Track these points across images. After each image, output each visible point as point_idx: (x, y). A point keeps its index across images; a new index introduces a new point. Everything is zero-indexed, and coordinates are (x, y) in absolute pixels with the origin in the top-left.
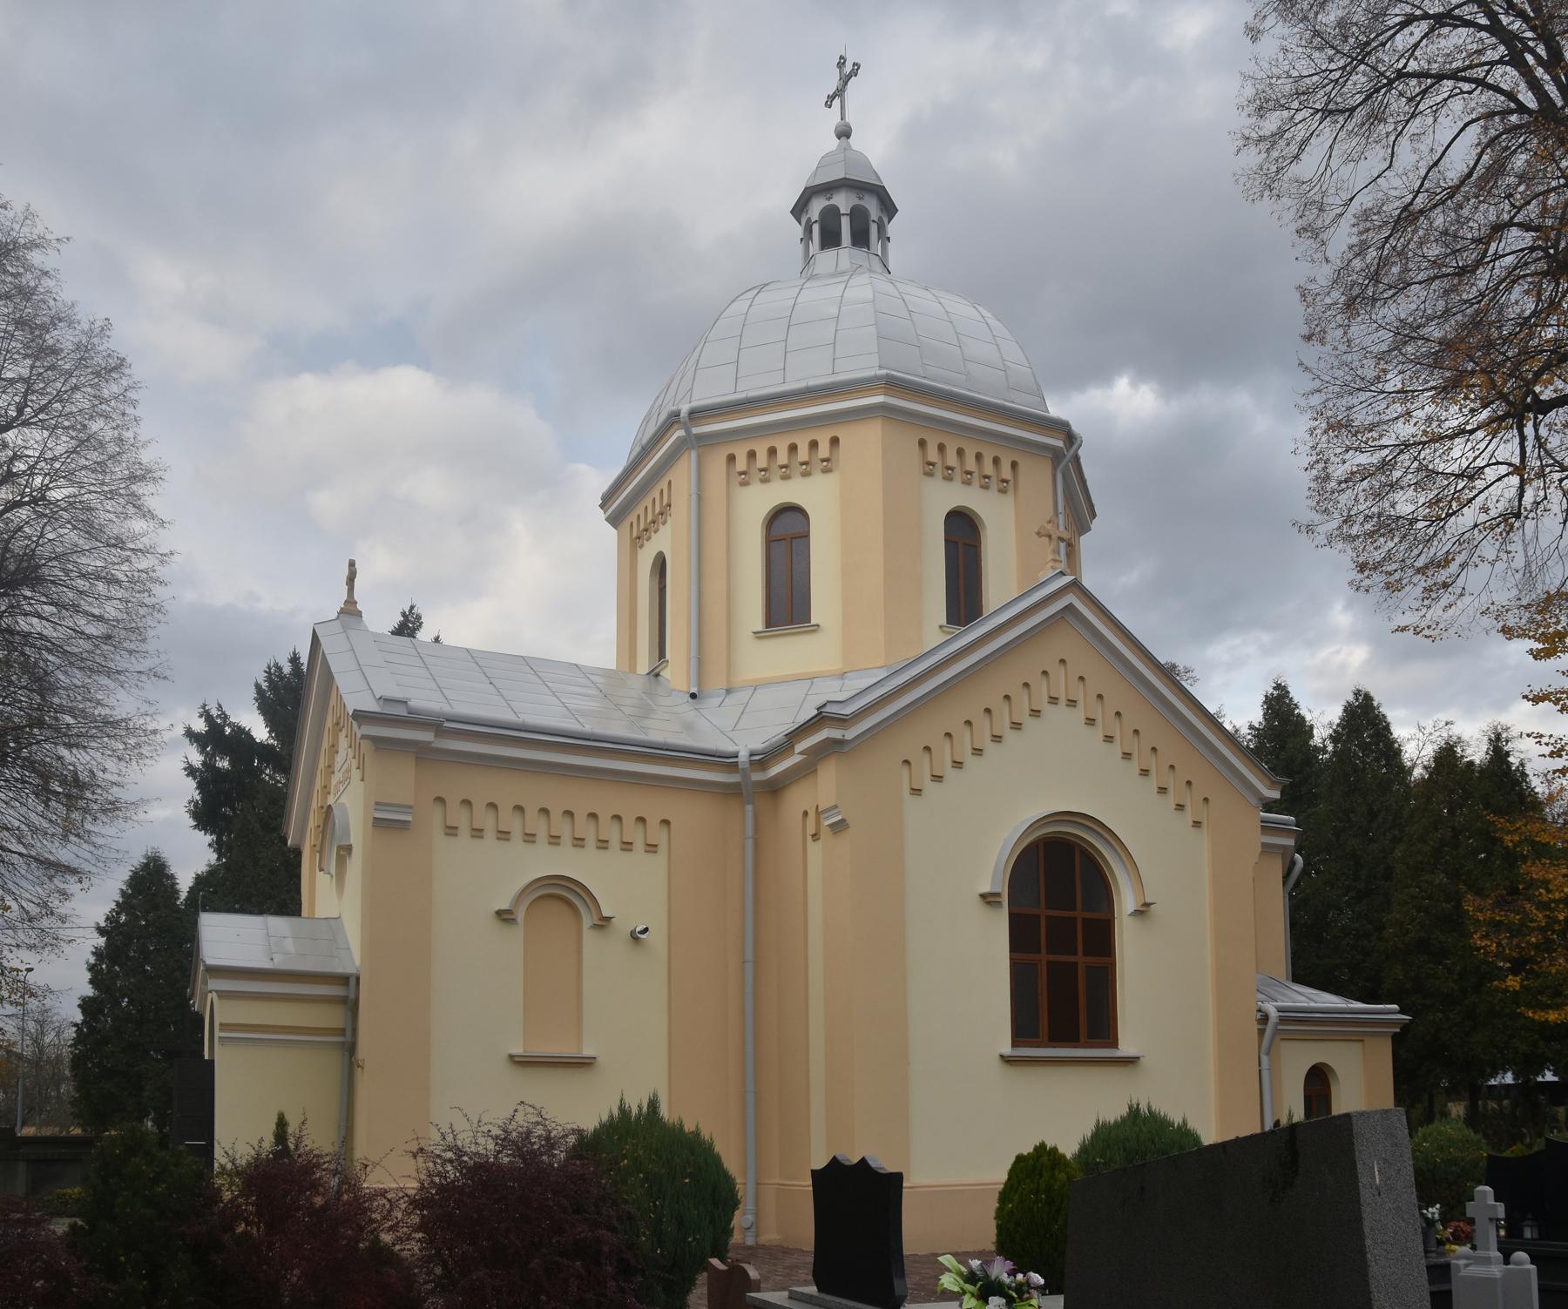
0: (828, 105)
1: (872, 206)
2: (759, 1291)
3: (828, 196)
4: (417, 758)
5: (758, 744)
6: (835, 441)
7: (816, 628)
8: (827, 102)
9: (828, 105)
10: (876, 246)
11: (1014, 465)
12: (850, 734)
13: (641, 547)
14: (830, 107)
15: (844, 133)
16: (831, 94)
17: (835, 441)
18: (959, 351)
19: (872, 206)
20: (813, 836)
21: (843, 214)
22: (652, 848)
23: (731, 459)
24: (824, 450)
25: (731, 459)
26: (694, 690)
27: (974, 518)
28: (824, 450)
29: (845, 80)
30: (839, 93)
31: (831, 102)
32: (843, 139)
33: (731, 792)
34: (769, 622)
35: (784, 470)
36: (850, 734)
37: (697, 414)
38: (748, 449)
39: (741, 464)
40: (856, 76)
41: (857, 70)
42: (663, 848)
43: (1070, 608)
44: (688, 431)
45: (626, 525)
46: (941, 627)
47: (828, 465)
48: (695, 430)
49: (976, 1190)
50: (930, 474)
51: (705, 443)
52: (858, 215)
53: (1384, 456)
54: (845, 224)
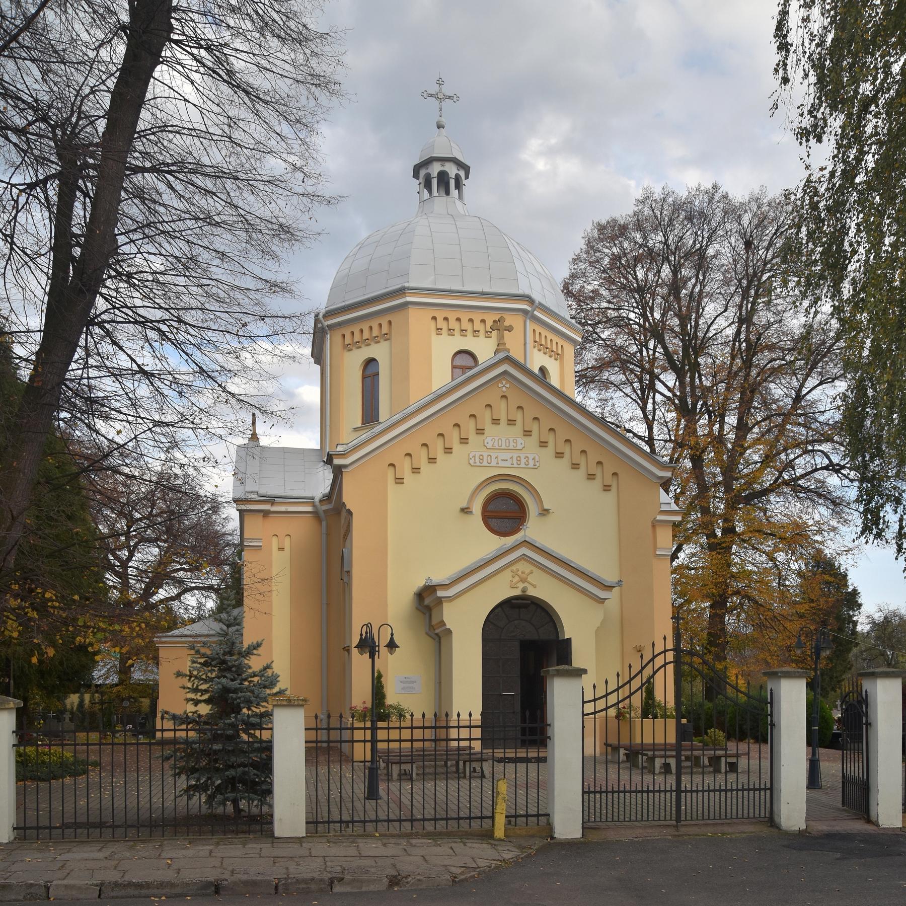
10: (454, 192)
17: (390, 322)
23: (344, 336)
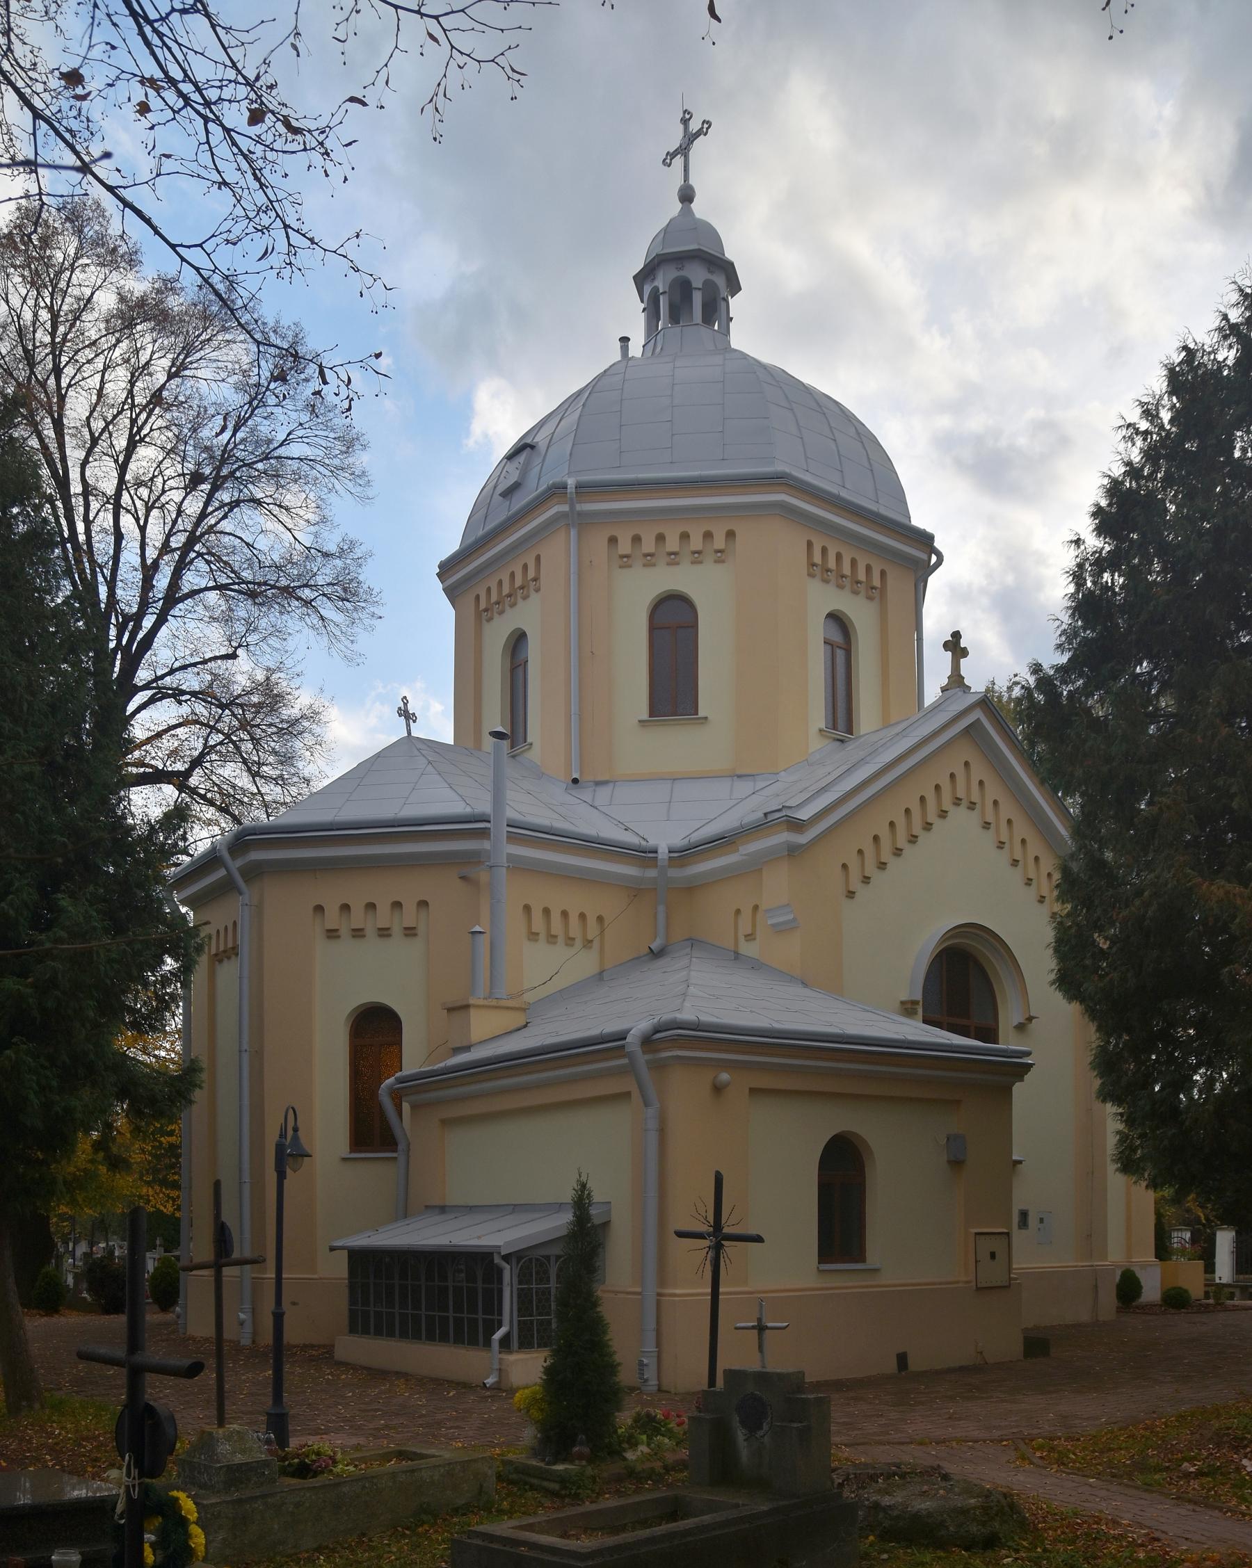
0: (667, 163)
1: (720, 281)
2: (804, 1393)
3: (680, 266)
4: (656, 852)
5: (678, 841)
6: (731, 535)
7: (704, 721)
8: (664, 160)
9: (667, 163)
11: (883, 573)
12: (803, 839)
13: (489, 620)
14: (669, 166)
15: (687, 196)
16: (671, 151)
17: (731, 535)
18: (834, 448)
19: (720, 281)
20: (746, 936)
21: (696, 289)
22: (410, 932)
23: (613, 540)
24: (719, 542)
25: (613, 540)
26: (575, 776)
27: (848, 626)
28: (719, 542)
29: (690, 138)
30: (683, 150)
31: (671, 160)
32: (687, 203)
33: (635, 891)
34: (653, 712)
35: (719, 554)
36: (803, 839)
37: (586, 490)
38: (657, 532)
39: (625, 546)
40: (705, 134)
41: (707, 129)
42: (596, 944)
43: (977, 724)
44: (572, 507)
45: (470, 599)
46: (821, 730)
47: (721, 556)
48: (578, 507)
49: (893, 1291)
50: (811, 575)
51: (584, 522)
52: (709, 288)
53: (136, 561)
54: (697, 298)
